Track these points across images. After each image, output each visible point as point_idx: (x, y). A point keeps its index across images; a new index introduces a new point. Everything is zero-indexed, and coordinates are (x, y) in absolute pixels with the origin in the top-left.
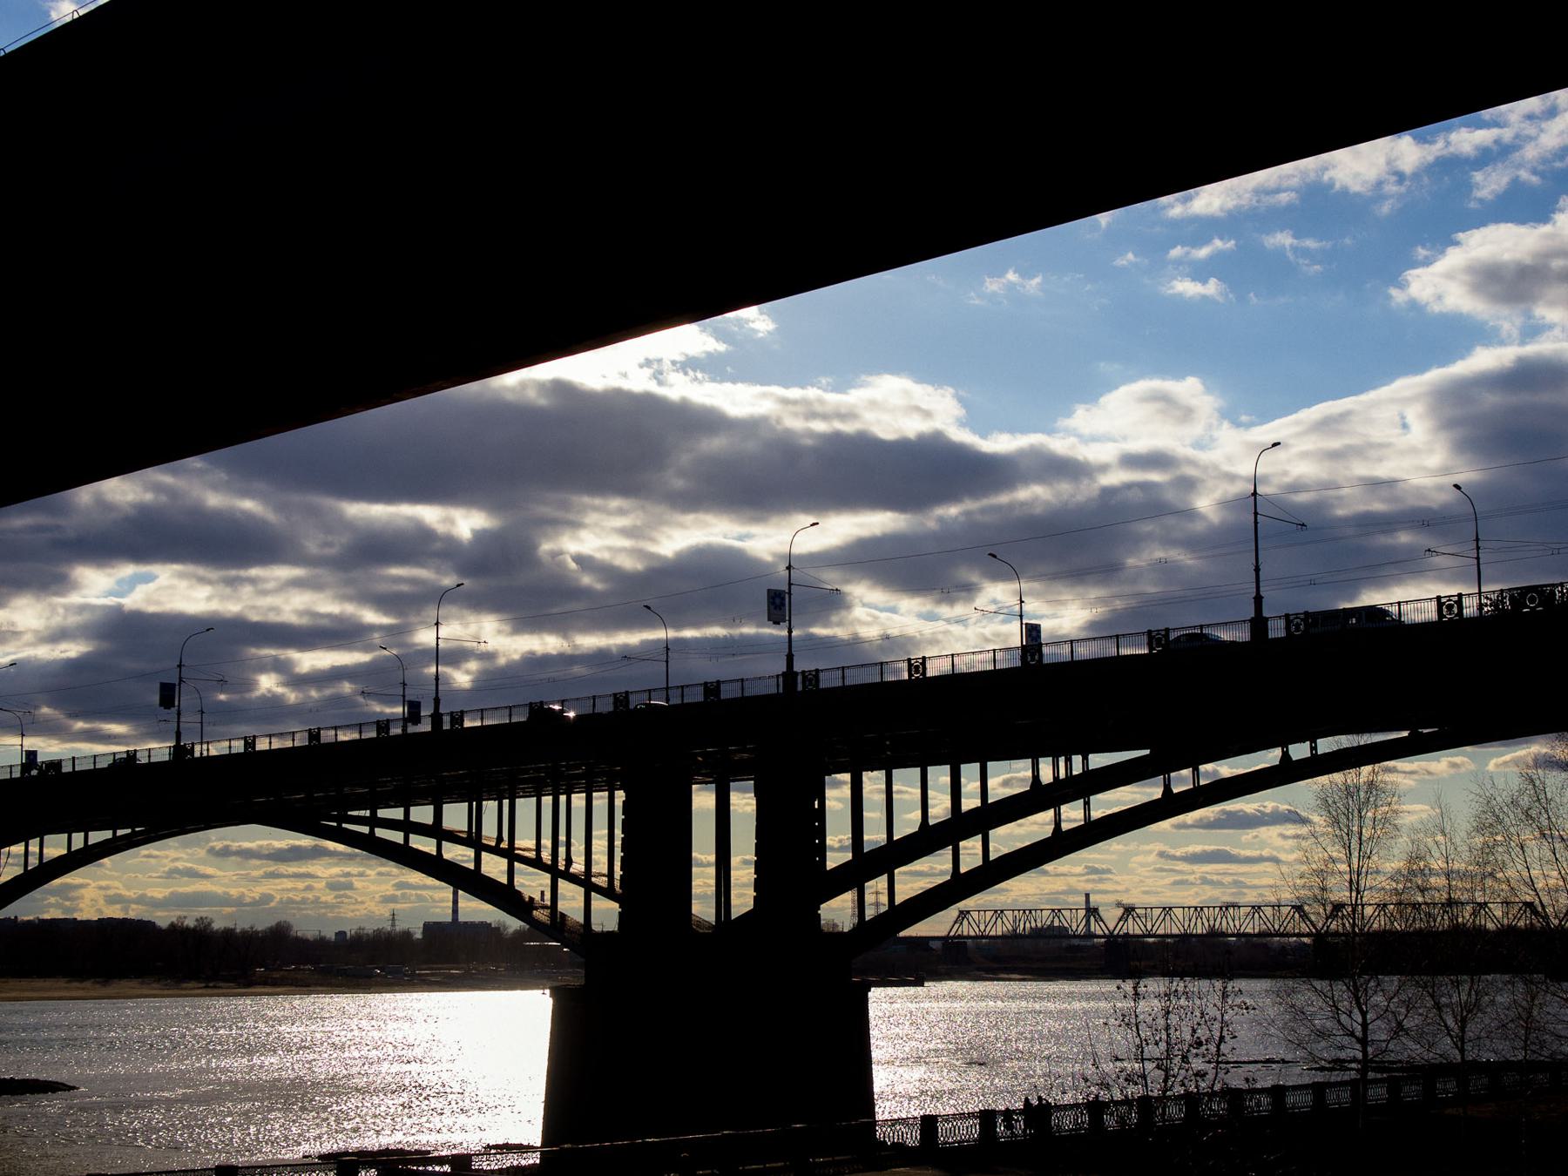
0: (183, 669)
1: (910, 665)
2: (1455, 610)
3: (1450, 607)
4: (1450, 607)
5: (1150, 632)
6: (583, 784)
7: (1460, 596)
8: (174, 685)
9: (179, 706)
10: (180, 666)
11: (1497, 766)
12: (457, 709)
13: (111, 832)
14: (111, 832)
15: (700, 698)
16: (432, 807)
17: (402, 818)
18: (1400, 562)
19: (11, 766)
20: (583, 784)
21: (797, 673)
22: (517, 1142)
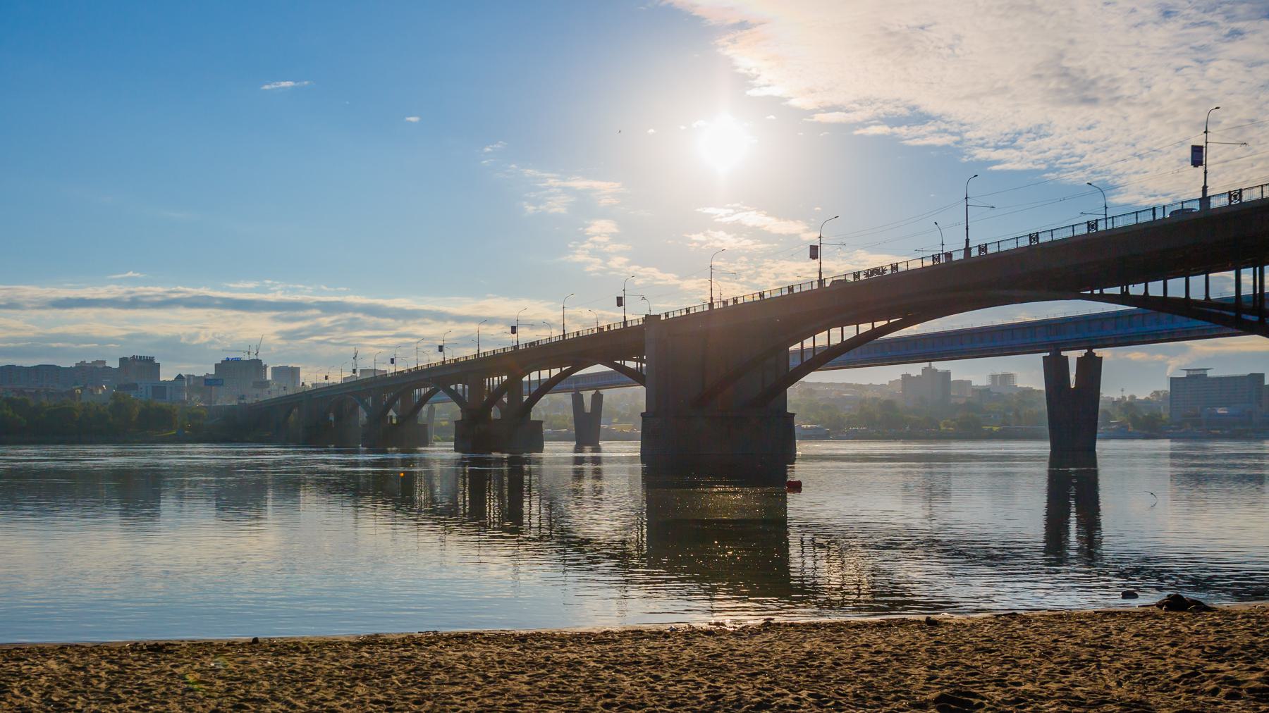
0: (968, 199)
1: (1089, 225)
2: (1238, 197)
3: (1235, 196)
4: (1235, 196)
5: (1088, 222)
6: (489, 380)
7: (1097, 220)
8: (1202, 147)
9: (1206, 165)
10: (966, 198)
11: (391, 417)
12: (688, 307)
13: (559, 369)
14: (559, 369)
15: (787, 293)
16: (1120, 293)
17: (1162, 295)
18: (967, 226)
19: (1154, 209)
20: (489, 380)
21: (239, 403)
22: (497, 629)
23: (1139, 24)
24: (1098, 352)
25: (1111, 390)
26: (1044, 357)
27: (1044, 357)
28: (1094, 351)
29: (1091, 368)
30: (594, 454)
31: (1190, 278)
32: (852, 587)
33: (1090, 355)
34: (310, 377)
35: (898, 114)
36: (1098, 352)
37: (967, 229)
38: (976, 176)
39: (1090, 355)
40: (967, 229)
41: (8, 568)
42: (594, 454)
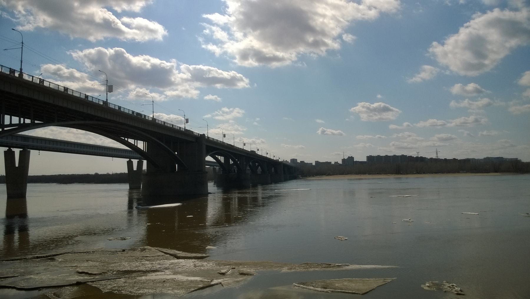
23: (372, 289)
24: (132, 160)
25: (33, 170)
26: (20, 151)
27: (20, 151)
28: (12, 148)
29: (25, 158)
30: (243, 195)
31: (18, 123)
32: (329, 12)
33: (130, 161)
34: (522, 161)
35: (171, 118)
36: (132, 160)
37: (21, 62)
38: (12, 29)
39: (130, 161)
40: (21, 62)
41: (275, 186)
42: (243, 195)
